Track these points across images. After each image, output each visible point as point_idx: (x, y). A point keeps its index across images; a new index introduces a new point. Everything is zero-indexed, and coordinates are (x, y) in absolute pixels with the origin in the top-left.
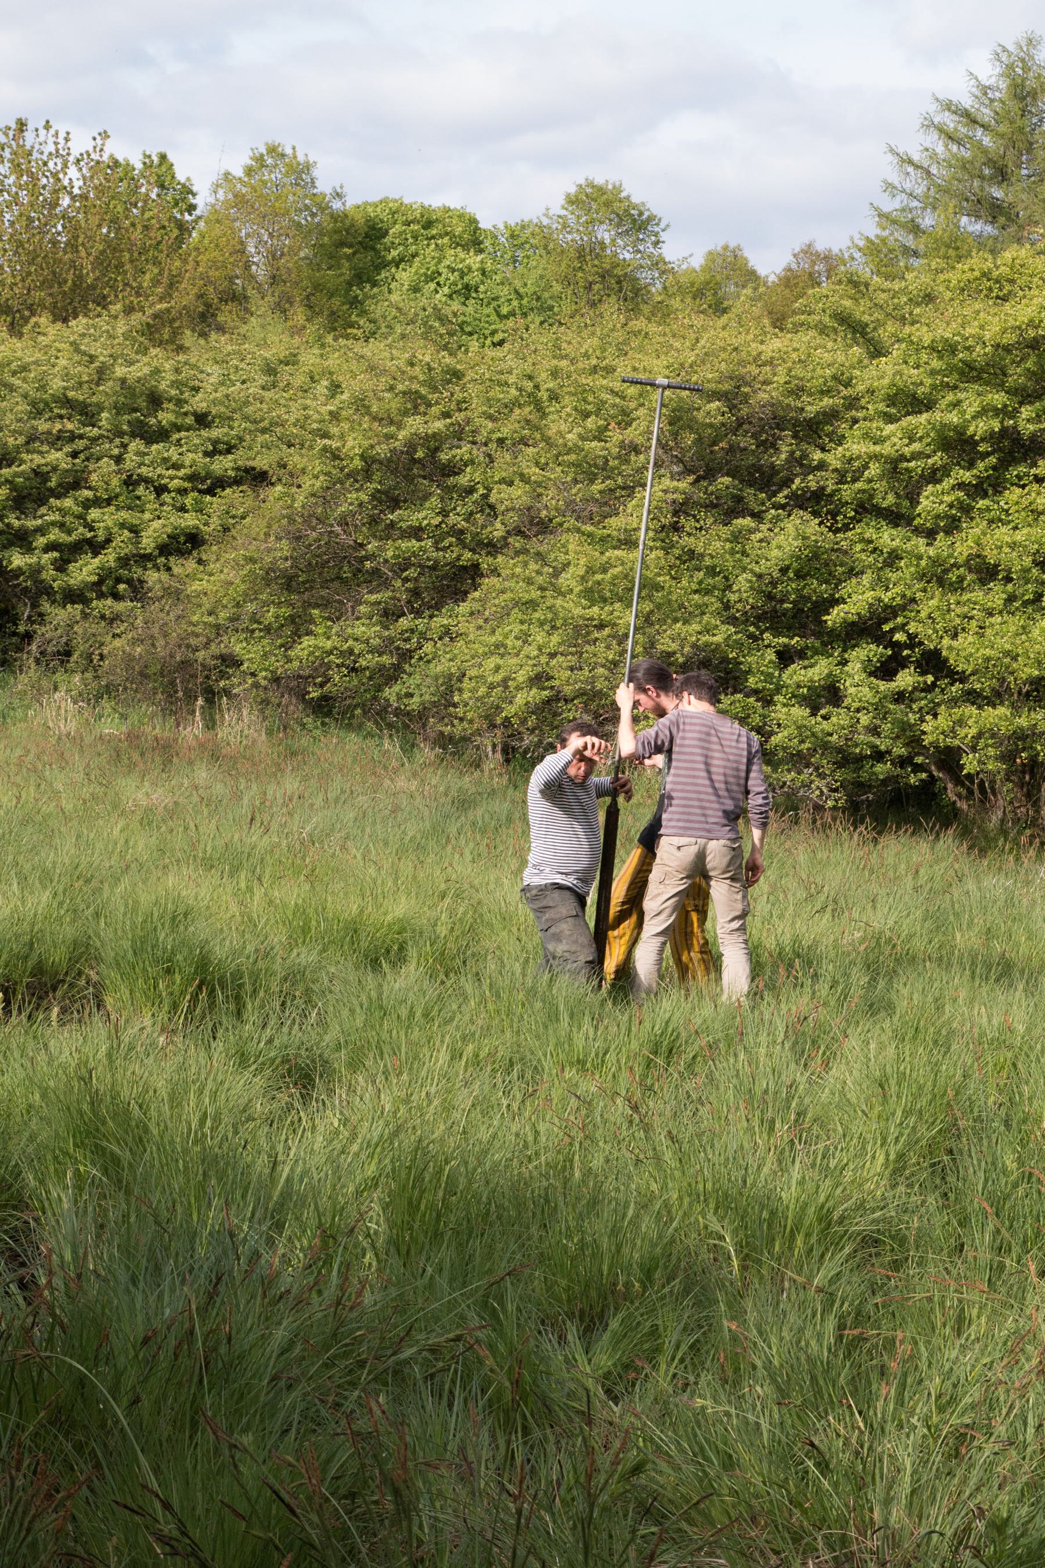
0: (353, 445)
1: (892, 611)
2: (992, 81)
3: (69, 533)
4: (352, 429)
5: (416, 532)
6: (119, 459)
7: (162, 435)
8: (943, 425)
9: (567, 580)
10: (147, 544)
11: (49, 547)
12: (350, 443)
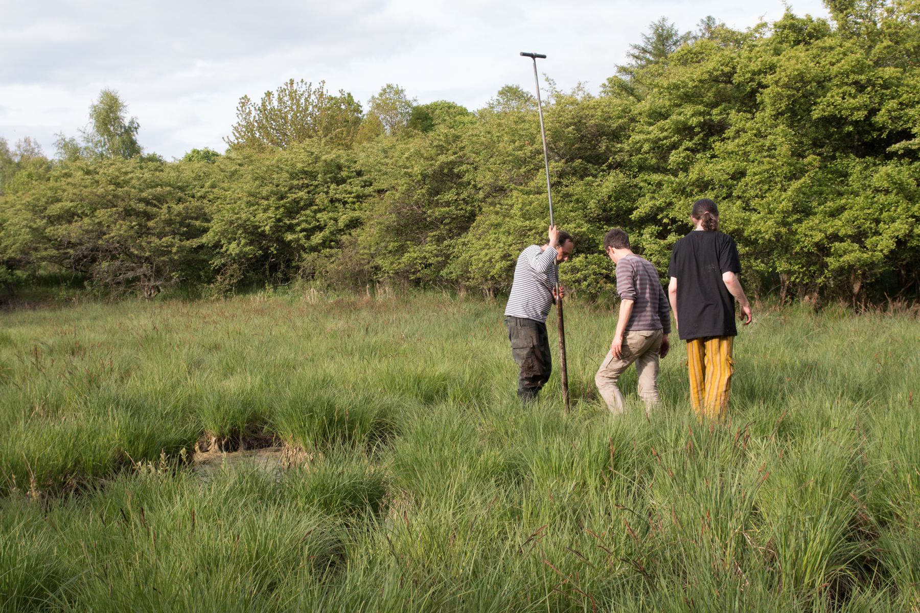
0: (417, 170)
1: (660, 209)
2: (651, 36)
3: (309, 224)
4: (416, 163)
5: (448, 204)
6: (327, 193)
7: (343, 181)
8: (678, 122)
9: (515, 211)
10: (341, 224)
11: (302, 231)
12: (415, 169)
